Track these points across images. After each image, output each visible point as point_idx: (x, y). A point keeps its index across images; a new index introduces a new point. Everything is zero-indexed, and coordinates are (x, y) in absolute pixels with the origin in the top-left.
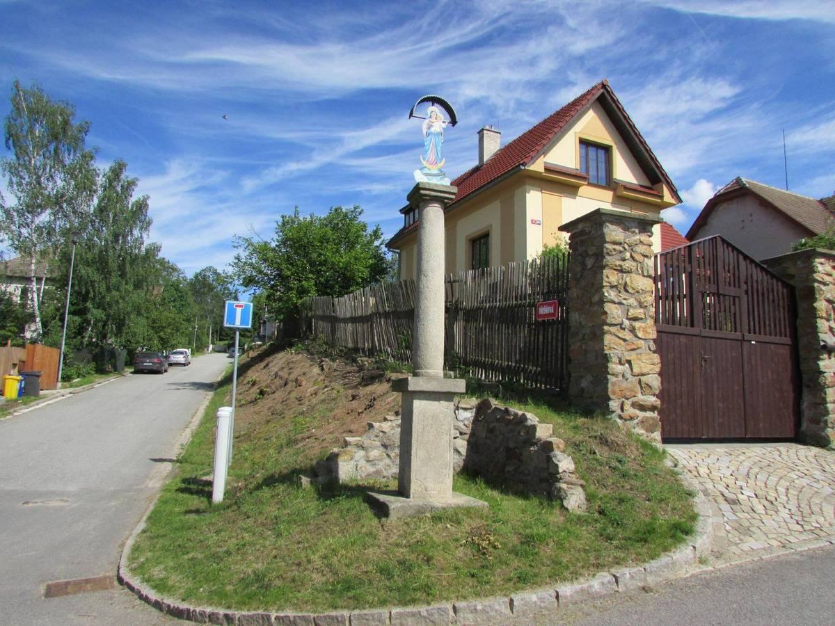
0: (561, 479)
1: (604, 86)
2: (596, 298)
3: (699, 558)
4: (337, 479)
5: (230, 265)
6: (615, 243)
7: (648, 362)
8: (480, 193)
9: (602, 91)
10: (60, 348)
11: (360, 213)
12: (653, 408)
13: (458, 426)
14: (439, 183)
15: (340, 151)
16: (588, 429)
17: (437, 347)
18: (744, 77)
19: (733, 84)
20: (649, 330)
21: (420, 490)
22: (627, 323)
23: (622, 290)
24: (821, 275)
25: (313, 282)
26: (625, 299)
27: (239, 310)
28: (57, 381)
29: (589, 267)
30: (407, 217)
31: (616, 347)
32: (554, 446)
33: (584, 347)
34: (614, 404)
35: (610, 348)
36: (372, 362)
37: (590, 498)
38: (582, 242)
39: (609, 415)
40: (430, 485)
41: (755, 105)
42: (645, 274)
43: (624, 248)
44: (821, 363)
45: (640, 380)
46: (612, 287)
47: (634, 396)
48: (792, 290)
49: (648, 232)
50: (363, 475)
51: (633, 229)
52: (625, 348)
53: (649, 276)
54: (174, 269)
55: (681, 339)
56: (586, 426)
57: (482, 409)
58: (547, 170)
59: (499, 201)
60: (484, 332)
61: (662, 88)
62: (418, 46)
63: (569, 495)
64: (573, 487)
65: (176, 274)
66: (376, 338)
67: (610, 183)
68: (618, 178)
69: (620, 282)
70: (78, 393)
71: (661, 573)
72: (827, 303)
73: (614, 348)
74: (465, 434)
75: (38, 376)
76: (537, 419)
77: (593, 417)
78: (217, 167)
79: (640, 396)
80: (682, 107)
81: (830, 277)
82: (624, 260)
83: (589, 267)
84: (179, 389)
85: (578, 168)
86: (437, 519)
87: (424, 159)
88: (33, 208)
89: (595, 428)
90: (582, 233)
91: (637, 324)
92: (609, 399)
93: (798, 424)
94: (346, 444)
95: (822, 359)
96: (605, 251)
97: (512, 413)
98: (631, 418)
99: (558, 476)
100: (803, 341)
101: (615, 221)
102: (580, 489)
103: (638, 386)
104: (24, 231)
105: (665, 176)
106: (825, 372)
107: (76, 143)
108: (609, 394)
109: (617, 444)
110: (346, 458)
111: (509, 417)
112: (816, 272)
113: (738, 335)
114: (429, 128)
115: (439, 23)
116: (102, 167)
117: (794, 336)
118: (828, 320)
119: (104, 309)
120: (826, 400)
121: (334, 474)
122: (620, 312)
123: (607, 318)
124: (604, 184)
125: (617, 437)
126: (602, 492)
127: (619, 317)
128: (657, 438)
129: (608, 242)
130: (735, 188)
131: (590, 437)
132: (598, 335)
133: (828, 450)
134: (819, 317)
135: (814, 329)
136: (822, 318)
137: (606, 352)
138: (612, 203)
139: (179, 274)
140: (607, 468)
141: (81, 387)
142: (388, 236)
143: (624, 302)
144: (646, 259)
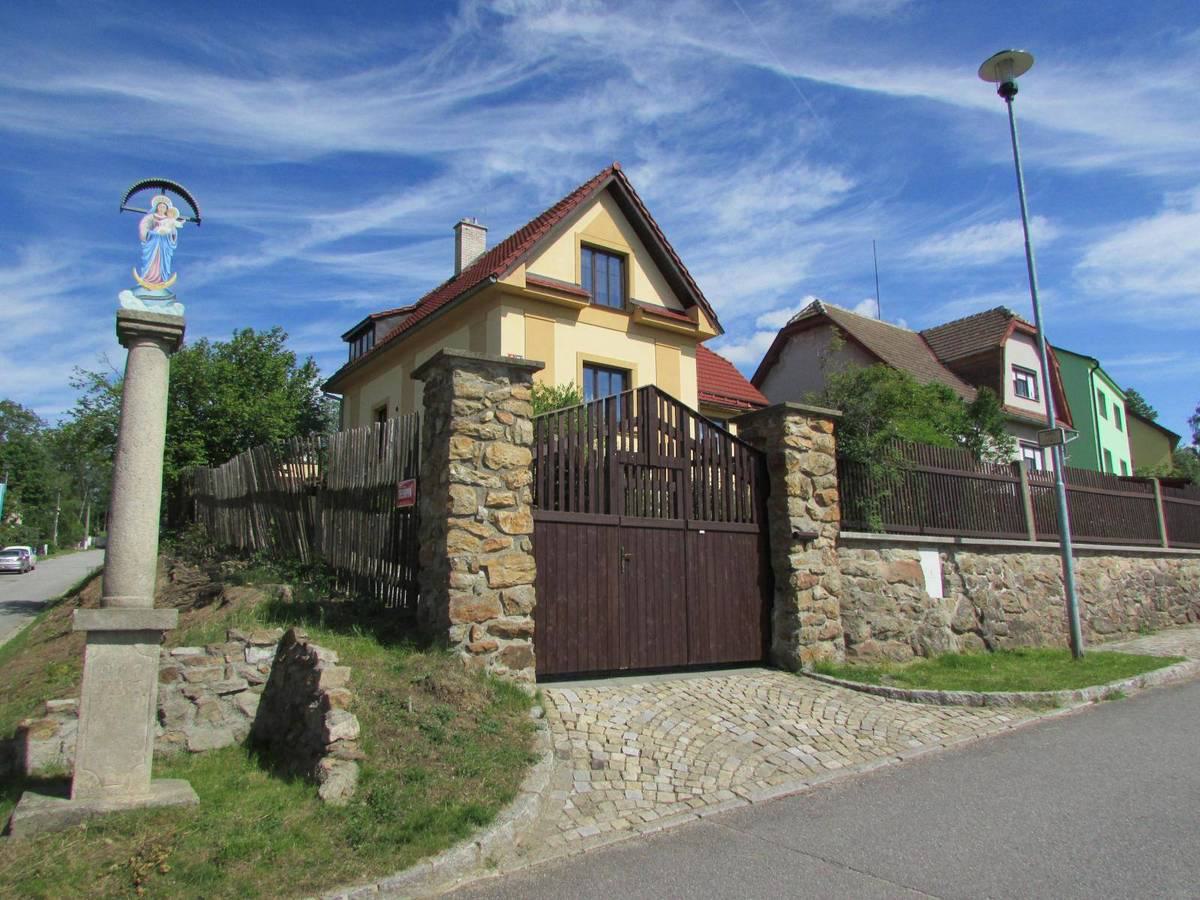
3: (487, 859)
4: (23, 767)
5: (69, 412)
6: (470, 398)
7: (515, 567)
8: (451, 309)
9: (612, 177)
11: (283, 339)
12: (523, 634)
13: (246, 673)
14: (164, 311)
15: (305, 242)
17: (137, 561)
18: (860, 166)
19: (846, 175)
20: (522, 522)
21: (90, 785)
22: (484, 512)
24: (795, 439)
25: (202, 443)
26: (482, 478)
30: (353, 345)
31: (466, 548)
34: (457, 632)
36: (243, 567)
39: (449, 646)
41: (876, 204)
42: (518, 441)
44: (793, 558)
45: (501, 594)
46: (464, 461)
47: (491, 618)
48: (761, 458)
49: (526, 381)
51: (501, 378)
52: (482, 549)
53: (525, 445)
55: (589, 531)
57: (286, 642)
61: (759, 175)
62: (425, 93)
65: (32, 426)
67: (625, 305)
68: (636, 298)
69: (476, 454)
71: (409, 890)
72: (803, 476)
73: (464, 550)
74: (258, 684)
79: (502, 618)
80: (784, 203)
81: (808, 441)
82: (483, 422)
85: (579, 282)
87: (140, 275)
91: (501, 514)
92: (450, 624)
93: (767, 640)
94: (48, 712)
95: (795, 552)
96: (453, 410)
97: (310, 652)
98: (486, 650)
100: (774, 528)
101: (472, 366)
102: (353, 766)
103: (499, 602)
105: (700, 296)
106: (797, 570)
112: (788, 435)
113: (680, 522)
115: (452, 65)
117: (764, 521)
118: (805, 499)
120: (797, 608)
122: (474, 498)
123: (453, 506)
124: (618, 306)
127: (471, 504)
128: (528, 676)
130: (813, 314)
133: (798, 676)
134: (792, 495)
135: (785, 509)
136: (795, 496)
138: (627, 333)
139: (38, 425)
140: (416, 728)
142: (325, 376)
143: (482, 482)
144: (519, 420)
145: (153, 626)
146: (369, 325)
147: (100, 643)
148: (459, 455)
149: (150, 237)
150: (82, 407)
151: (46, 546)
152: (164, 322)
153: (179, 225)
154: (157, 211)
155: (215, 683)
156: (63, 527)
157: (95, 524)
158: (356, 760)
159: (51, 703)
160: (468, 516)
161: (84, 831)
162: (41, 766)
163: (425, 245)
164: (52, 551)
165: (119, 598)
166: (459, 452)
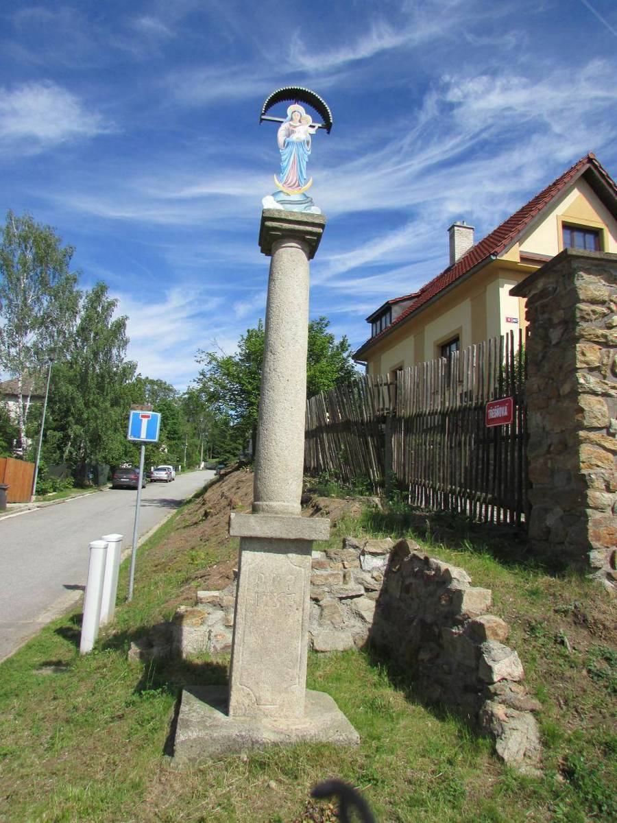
0: (496, 694)
1: (590, 160)
2: (566, 388)
4: (179, 652)
6: (594, 302)
9: (588, 166)
10: (35, 462)
11: (326, 326)
16: (554, 595)
17: (287, 466)
21: (247, 702)
23: (609, 374)
27: (145, 421)
28: (32, 494)
29: (554, 342)
30: (374, 325)
31: (600, 464)
32: (488, 633)
33: (549, 465)
35: (591, 466)
37: (548, 739)
38: (544, 306)
40: (266, 695)
43: (609, 308)
46: (591, 370)
50: (218, 647)
54: (171, 390)
56: (552, 590)
57: (398, 553)
58: (523, 259)
59: (468, 300)
60: (424, 447)
62: (403, 165)
63: (508, 732)
64: (515, 713)
65: (172, 395)
66: (320, 456)
69: (605, 361)
70: (45, 507)
73: (598, 466)
75: (5, 489)
76: (469, 579)
77: (564, 576)
78: (212, 293)
83: (554, 342)
84: (144, 506)
86: (259, 765)
88: (21, 329)
89: (566, 594)
90: (543, 293)
92: (591, 548)
94: (198, 602)
96: (578, 314)
97: (434, 566)
99: (491, 687)
101: (594, 268)
102: (530, 718)
104: (13, 351)
107: (60, 266)
108: (590, 539)
109: (604, 625)
110: (194, 620)
111: (428, 572)
114: (288, 135)
115: (419, 143)
116: (85, 289)
119: (83, 426)
121: (175, 644)
122: (605, 409)
123: (584, 418)
125: (604, 613)
126: (572, 726)
127: (603, 416)
129: (584, 301)
131: (556, 611)
132: (570, 446)
137: (584, 472)
140: (584, 672)
141: (52, 501)
142: (354, 349)
145: (306, 537)
146: (386, 309)
147: (254, 550)
148: (587, 363)
149: (287, 144)
150: (202, 377)
151: (180, 467)
152: (306, 220)
153: (313, 131)
154: (292, 119)
155: (336, 587)
156: (189, 456)
157: (206, 455)
158: (532, 711)
159: (202, 594)
160: (599, 429)
161: (245, 763)
162: (193, 651)
163: (406, 268)
164: (183, 470)
165: (271, 503)
166: (587, 359)
